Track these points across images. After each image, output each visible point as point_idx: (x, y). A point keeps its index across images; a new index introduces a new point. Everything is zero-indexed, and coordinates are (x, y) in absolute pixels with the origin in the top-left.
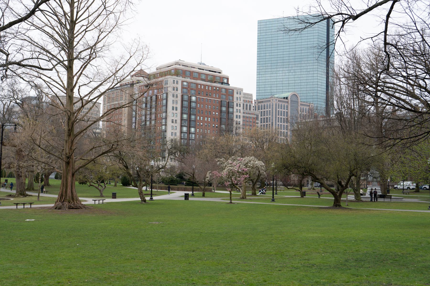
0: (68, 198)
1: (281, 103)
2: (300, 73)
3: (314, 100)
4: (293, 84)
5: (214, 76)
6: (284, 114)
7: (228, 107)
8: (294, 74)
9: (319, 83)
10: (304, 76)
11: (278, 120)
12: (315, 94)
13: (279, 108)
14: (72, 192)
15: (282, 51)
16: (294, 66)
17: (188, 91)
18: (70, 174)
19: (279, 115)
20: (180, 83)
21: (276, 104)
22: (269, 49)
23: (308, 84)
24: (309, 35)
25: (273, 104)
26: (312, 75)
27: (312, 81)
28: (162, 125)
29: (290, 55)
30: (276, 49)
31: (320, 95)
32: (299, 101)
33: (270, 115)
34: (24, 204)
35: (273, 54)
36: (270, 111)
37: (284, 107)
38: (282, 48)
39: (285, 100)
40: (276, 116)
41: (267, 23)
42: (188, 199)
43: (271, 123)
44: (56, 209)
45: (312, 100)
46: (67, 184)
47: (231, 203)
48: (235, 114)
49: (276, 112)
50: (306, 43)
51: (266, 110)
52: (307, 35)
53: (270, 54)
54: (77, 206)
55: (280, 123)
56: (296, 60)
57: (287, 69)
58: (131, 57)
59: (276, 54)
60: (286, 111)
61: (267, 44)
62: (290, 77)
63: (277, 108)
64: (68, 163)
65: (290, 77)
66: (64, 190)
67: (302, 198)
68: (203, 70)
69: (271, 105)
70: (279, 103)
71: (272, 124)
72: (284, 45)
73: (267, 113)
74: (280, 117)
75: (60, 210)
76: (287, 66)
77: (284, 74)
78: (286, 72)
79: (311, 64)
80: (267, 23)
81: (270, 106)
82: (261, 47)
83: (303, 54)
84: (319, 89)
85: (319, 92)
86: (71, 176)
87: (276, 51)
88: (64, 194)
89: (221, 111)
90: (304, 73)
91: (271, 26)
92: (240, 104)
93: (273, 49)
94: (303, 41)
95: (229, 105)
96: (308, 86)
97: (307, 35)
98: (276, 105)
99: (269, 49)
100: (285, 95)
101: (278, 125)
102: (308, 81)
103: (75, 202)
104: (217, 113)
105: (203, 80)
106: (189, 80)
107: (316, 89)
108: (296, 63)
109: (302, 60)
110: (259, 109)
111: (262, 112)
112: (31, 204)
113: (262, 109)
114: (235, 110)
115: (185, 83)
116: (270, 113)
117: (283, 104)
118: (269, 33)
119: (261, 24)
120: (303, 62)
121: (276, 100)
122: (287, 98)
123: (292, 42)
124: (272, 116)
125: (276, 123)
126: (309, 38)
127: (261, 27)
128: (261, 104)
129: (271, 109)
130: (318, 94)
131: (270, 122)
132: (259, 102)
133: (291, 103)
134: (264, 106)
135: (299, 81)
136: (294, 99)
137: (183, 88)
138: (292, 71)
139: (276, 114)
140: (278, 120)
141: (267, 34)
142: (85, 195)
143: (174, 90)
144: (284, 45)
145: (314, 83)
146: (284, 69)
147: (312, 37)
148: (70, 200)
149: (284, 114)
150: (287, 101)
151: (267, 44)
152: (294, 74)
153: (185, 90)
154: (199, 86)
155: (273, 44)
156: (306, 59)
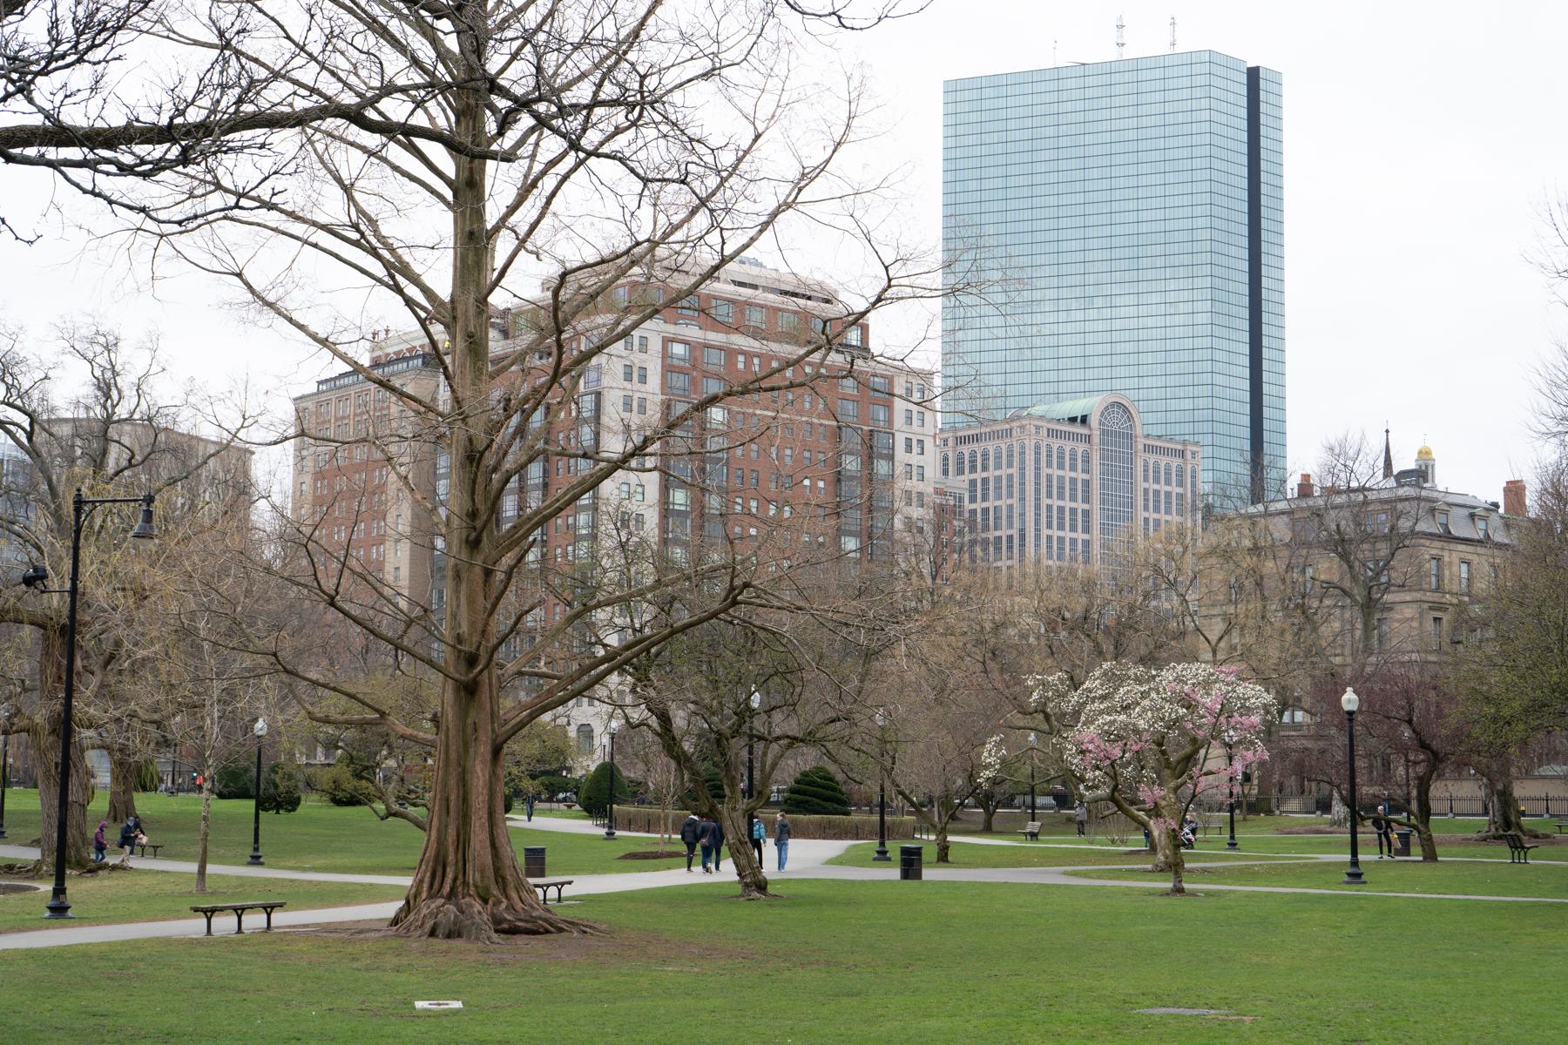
0: (473, 876)
1: (1060, 442)
2: (1132, 311)
3: (1200, 427)
4: (1106, 361)
5: (805, 316)
6: (1073, 490)
7: (871, 458)
8: (1106, 313)
9: (1218, 355)
10: (1150, 322)
11: (1049, 517)
12: (1202, 403)
13: (1049, 465)
14: (494, 846)
15: (1052, 212)
16: (1105, 278)
17: (693, 382)
18: (484, 749)
19: (1049, 495)
20: (655, 344)
21: (1037, 447)
22: (996, 206)
23: (1172, 356)
24: (1170, 143)
25: (1023, 447)
26: (1188, 319)
27: (1188, 343)
28: (577, 539)
29: (1090, 232)
30: (1027, 203)
31: (1226, 405)
32: (1139, 431)
33: (1010, 495)
34: (239, 911)
35: (1011, 228)
36: (1010, 477)
37: (1073, 459)
38: (1053, 201)
39: (1077, 429)
40: (1037, 499)
41: (987, 93)
42: (918, 876)
43: (1015, 532)
44: (433, 933)
45: (1188, 428)
46: (465, 799)
47: (1179, 890)
48: (901, 484)
49: (1037, 484)
50: (1159, 179)
51: (991, 473)
52: (1161, 143)
53: (1002, 228)
54: (533, 920)
55: (1056, 533)
56: (1117, 253)
57: (1078, 292)
58: (758, 137)
59: (1027, 226)
60: (1081, 476)
61: (986, 184)
62: (1089, 326)
63: (1043, 464)
64: (469, 691)
65: (1089, 326)
66: (452, 832)
67: (1429, 866)
68: (755, 287)
69: (1016, 449)
70: (1050, 440)
71: (1022, 537)
72: (1062, 188)
73: (998, 488)
74: (1056, 503)
75: (457, 943)
76: (1078, 280)
77: (1063, 316)
78: (1074, 304)
79: (1182, 272)
80: (987, 93)
81: (1010, 456)
82: (961, 198)
83: (1144, 228)
84: (1218, 379)
85: (1218, 391)
86: (489, 757)
87: (1027, 215)
88: (451, 857)
89: (838, 478)
90: (1154, 310)
91: (1002, 103)
92: (921, 442)
93: (1012, 204)
94: (1144, 168)
95: (873, 447)
96: (1172, 368)
97: (1161, 143)
98: (1038, 453)
99: (996, 206)
100: (1076, 407)
101: (1049, 538)
102: (1170, 345)
103: (514, 895)
104: (821, 484)
105: (756, 334)
106: (693, 332)
107: (1207, 378)
108: (1116, 265)
109: (1142, 251)
110: (960, 472)
111: (973, 483)
112: (269, 909)
113: (973, 469)
114: (899, 469)
115: (678, 349)
116: (1010, 486)
117: (1068, 446)
118: (995, 138)
119: (960, 96)
120: (1145, 262)
121: (1037, 427)
122: (1084, 420)
123: (1095, 173)
124: (1022, 499)
125: (1037, 530)
126: (1170, 154)
127: (960, 108)
128: (975, 446)
129: (1014, 471)
130: (1217, 403)
131: (1010, 526)
132: (961, 441)
133: (1102, 442)
134: (985, 455)
135: (1131, 347)
136: (1117, 423)
137: (668, 369)
138: (1099, 302)
139: (1038, 491)
140: (1049, 517)
141: (987, 138)
142: (339, 860)
143: (628, 377)
144: (1062, 188)
145: (1198, 355)
146: (1065, 293)
147: (1186, 153)
148: (487, 889)
149: (1073, 490)
150: (1085, 431)
151: (986, 184)
152: (1106, 313)
153: (679, 381)
154: (741, 358)
155: (1012, 182)
156: (1159, 250)
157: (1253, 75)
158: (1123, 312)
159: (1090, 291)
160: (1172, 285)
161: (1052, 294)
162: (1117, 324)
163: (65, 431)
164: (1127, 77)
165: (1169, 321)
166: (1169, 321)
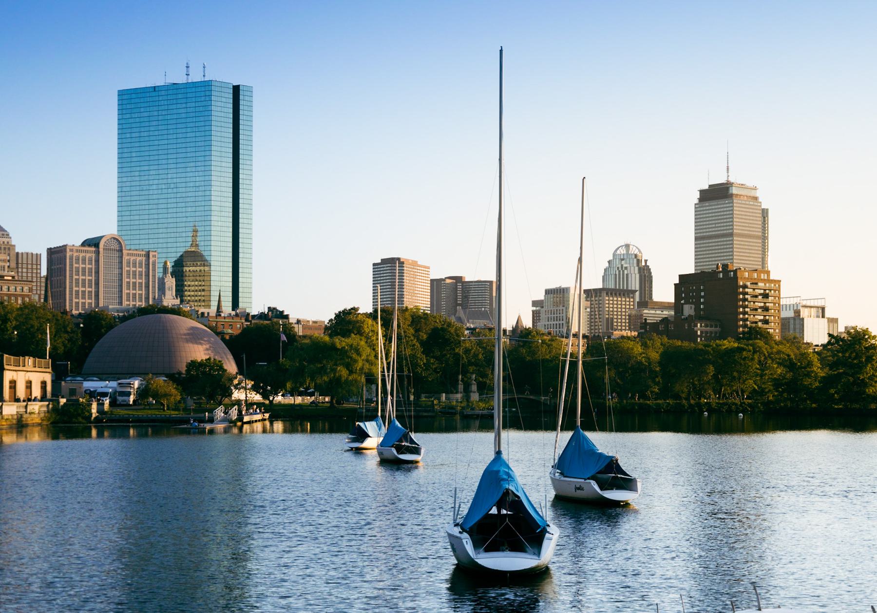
8: (175, 190)
16: (175, 175)
77: (160, 192)
78: (163, 186)
82: (124, 141)
96: (197, 214)
157: (236, 89)
158: (181, 190)
159: (170, 181)
160: (198, 179)
161: (156, 182)
162: (179, 195)
163: (460, 351)
164: (183, 91)
165: (197, 194)
166: (197, 194)
